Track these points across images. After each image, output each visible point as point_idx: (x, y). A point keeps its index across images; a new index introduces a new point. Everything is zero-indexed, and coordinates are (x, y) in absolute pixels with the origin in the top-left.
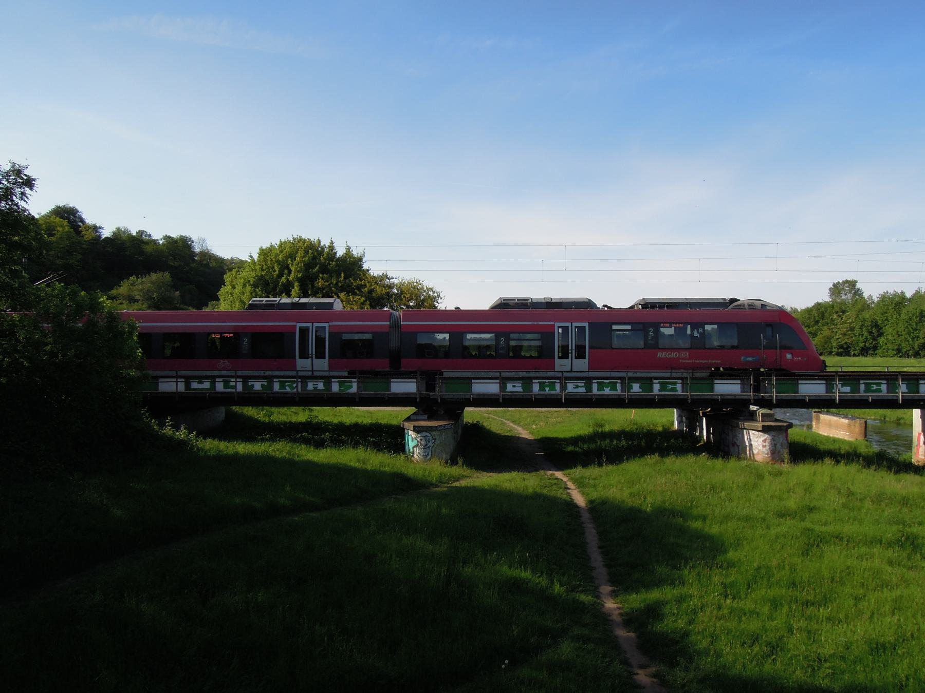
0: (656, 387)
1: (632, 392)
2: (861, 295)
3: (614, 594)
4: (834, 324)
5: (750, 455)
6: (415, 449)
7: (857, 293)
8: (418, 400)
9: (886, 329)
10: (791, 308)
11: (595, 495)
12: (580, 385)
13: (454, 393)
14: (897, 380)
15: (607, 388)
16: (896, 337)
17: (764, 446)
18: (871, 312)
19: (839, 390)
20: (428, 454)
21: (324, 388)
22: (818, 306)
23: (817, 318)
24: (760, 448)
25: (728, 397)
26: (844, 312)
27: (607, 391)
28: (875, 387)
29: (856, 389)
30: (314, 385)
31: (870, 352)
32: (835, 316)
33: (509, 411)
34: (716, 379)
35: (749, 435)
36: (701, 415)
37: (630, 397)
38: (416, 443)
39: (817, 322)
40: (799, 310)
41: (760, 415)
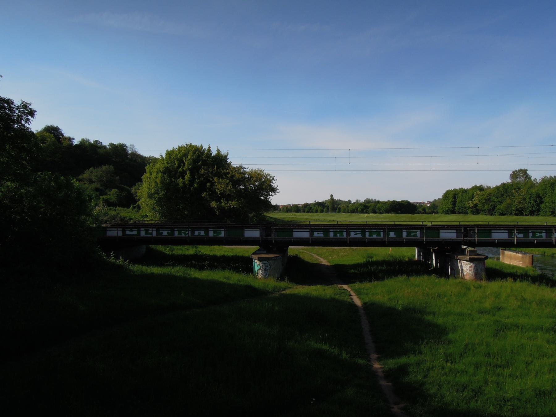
0: (405, 234)
1: (314, 237)
2: (530, 178)
3: (379, 360)
4: (513, 196)
5: (462, 276)
6: (259, 271)
7: (528, 177)
8: (261, 241)
9: (545, 199)
10: (487, 186)
11: (367, 300)
12: (358, 233)
13: (282, 238)
14: (552, 230)
15: (375, 234)
16: (551, 204)
17: (470, 270)
18: (536, 189)
19: (516, 236)
20: (267, 274)
21: (204, 234)
22: (503, 185)
23: (503, 193)
24: (468, 271)
25: (449, 240)
26: (519, 189)
27: (375, 236)
28: (538, 234)
29: (526, 236)
30: (198, 232)
31: (536, 213)
32: (514, 191)
33: (315, 248)
34: (493, 230)
35: (461, 263)
36: (432, 251)
37: (388, 240)
38: (260, 268)
39: (503, 195)
40: (492, 188)
41: (468, 251)
